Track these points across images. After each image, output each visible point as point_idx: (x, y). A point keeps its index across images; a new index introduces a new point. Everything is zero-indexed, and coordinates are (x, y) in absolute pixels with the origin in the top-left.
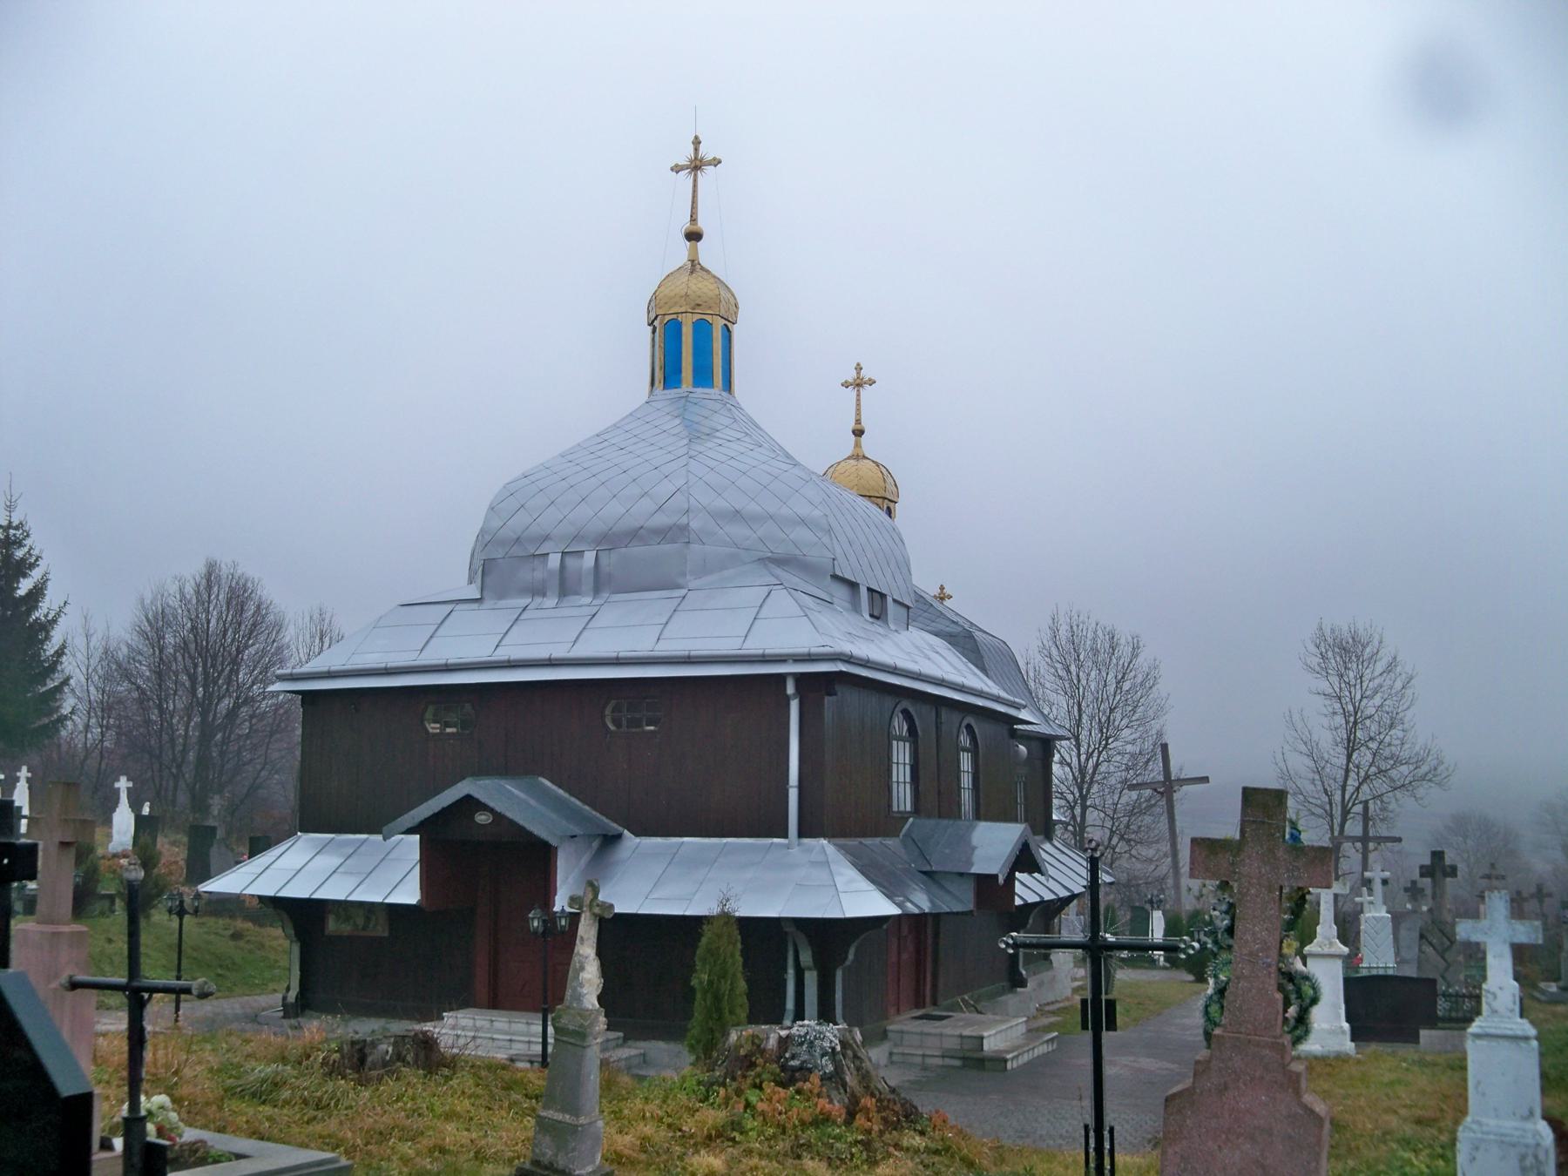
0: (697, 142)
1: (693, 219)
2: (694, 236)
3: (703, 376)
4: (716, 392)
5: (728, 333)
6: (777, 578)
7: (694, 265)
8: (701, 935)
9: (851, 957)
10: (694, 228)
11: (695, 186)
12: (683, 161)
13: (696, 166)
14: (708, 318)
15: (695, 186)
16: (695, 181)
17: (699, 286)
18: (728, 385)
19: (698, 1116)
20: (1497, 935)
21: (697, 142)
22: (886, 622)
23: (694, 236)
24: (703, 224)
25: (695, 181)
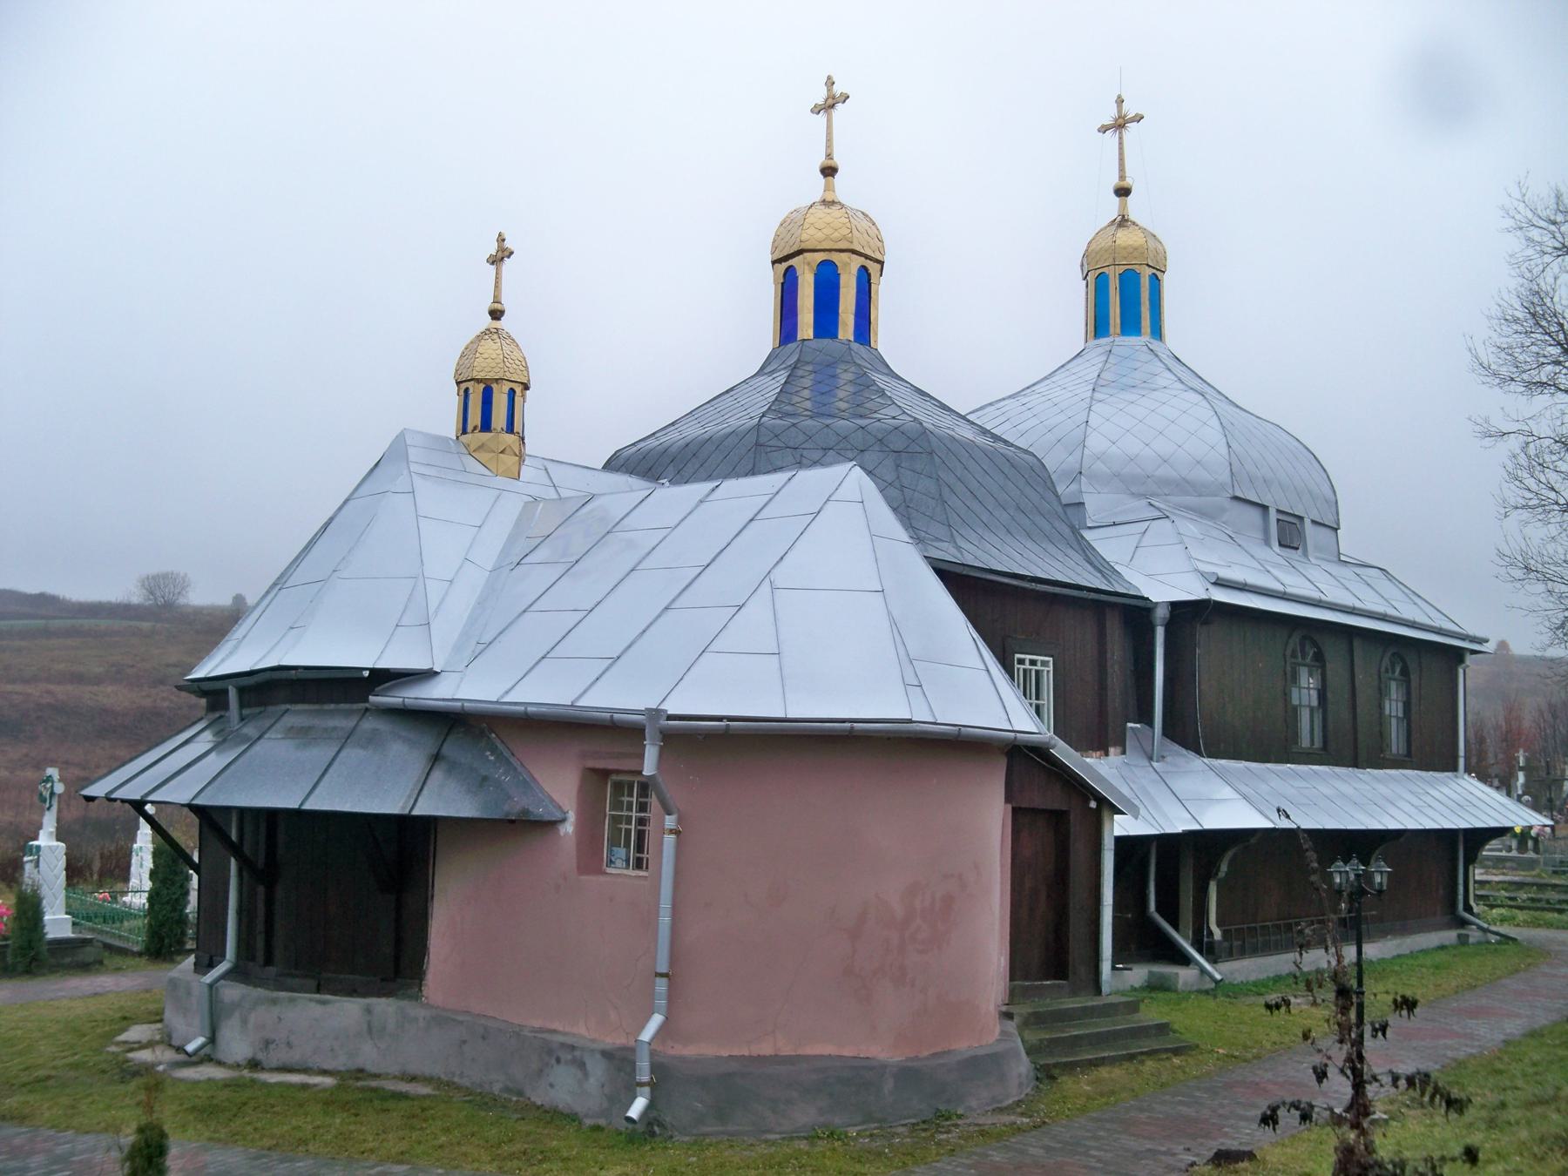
0: (1120, 101)
1: (1122, 177)
2: (829, 171)
3: (1130, 325)
4: (1145, 338)
5: (1156, 281)
6: (1159, 509)
7: (1123, 222)
8: (153, 875)
9: (1224, 868)
10: (830, 163)
11: (1121, 143)
12: (1108, 121)
13: (1120, 124)
14: (835, 257)
15: (1121, 143)
16: (1121, 138)
17: (1125, 237)
18: (1157, 332)
19: (613, 1040)
20: (95, 877)
21: (1120, 101)
22: (1305, 554)
23: (829, 171)
24: (838, 160)
25: (1121, 138)
